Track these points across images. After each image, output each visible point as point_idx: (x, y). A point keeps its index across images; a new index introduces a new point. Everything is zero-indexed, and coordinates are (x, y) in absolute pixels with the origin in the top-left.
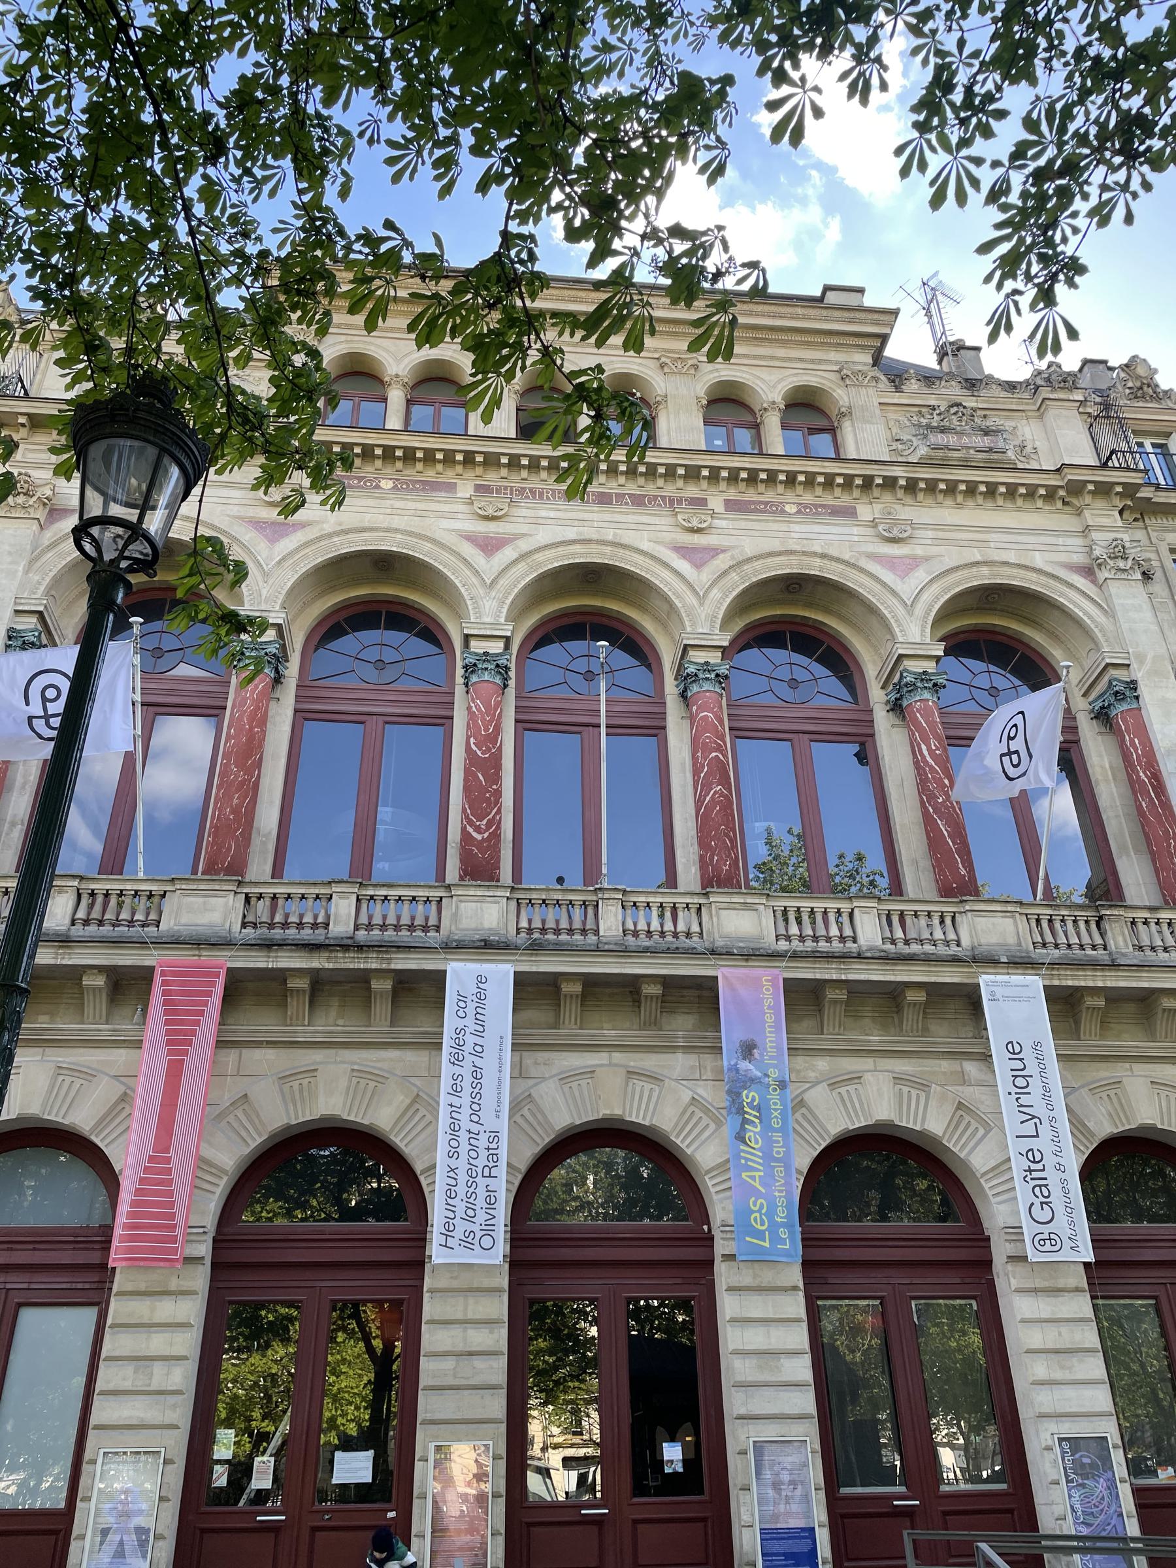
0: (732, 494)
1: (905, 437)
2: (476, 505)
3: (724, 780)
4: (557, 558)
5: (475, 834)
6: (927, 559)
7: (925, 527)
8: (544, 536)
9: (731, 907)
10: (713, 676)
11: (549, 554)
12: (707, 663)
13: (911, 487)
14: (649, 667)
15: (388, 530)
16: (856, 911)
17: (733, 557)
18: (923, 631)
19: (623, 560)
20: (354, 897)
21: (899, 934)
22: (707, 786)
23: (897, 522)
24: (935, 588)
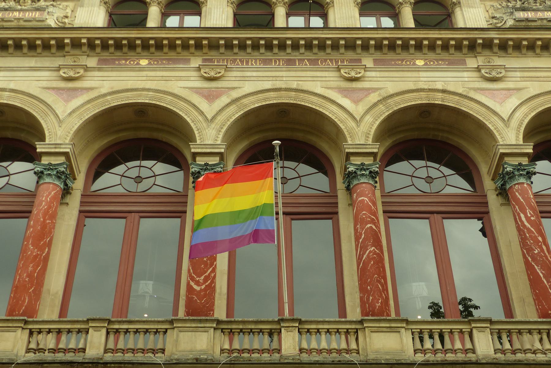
0: (378, 55)
1: (498, 15)
2: (202, 71)
3: (377, 243)
4: (258, 101)
5: (195, 287)
6: (519, 90)
7: (515, 70)
8: (248, 87)
9: (379, 330)
10: (367, 172)
11: (252, 98)
12: (363, 164)
13: (503, 46)
14: (325, 173)
15: (144, 89)
16: (475, 331)
17: (380, 95)
18: (517, 137)
19: (303, 100)
20: (104, 331)
21: (507, 346)
22: (364, 248)
23: (494, 67)
24: (524, 109)
